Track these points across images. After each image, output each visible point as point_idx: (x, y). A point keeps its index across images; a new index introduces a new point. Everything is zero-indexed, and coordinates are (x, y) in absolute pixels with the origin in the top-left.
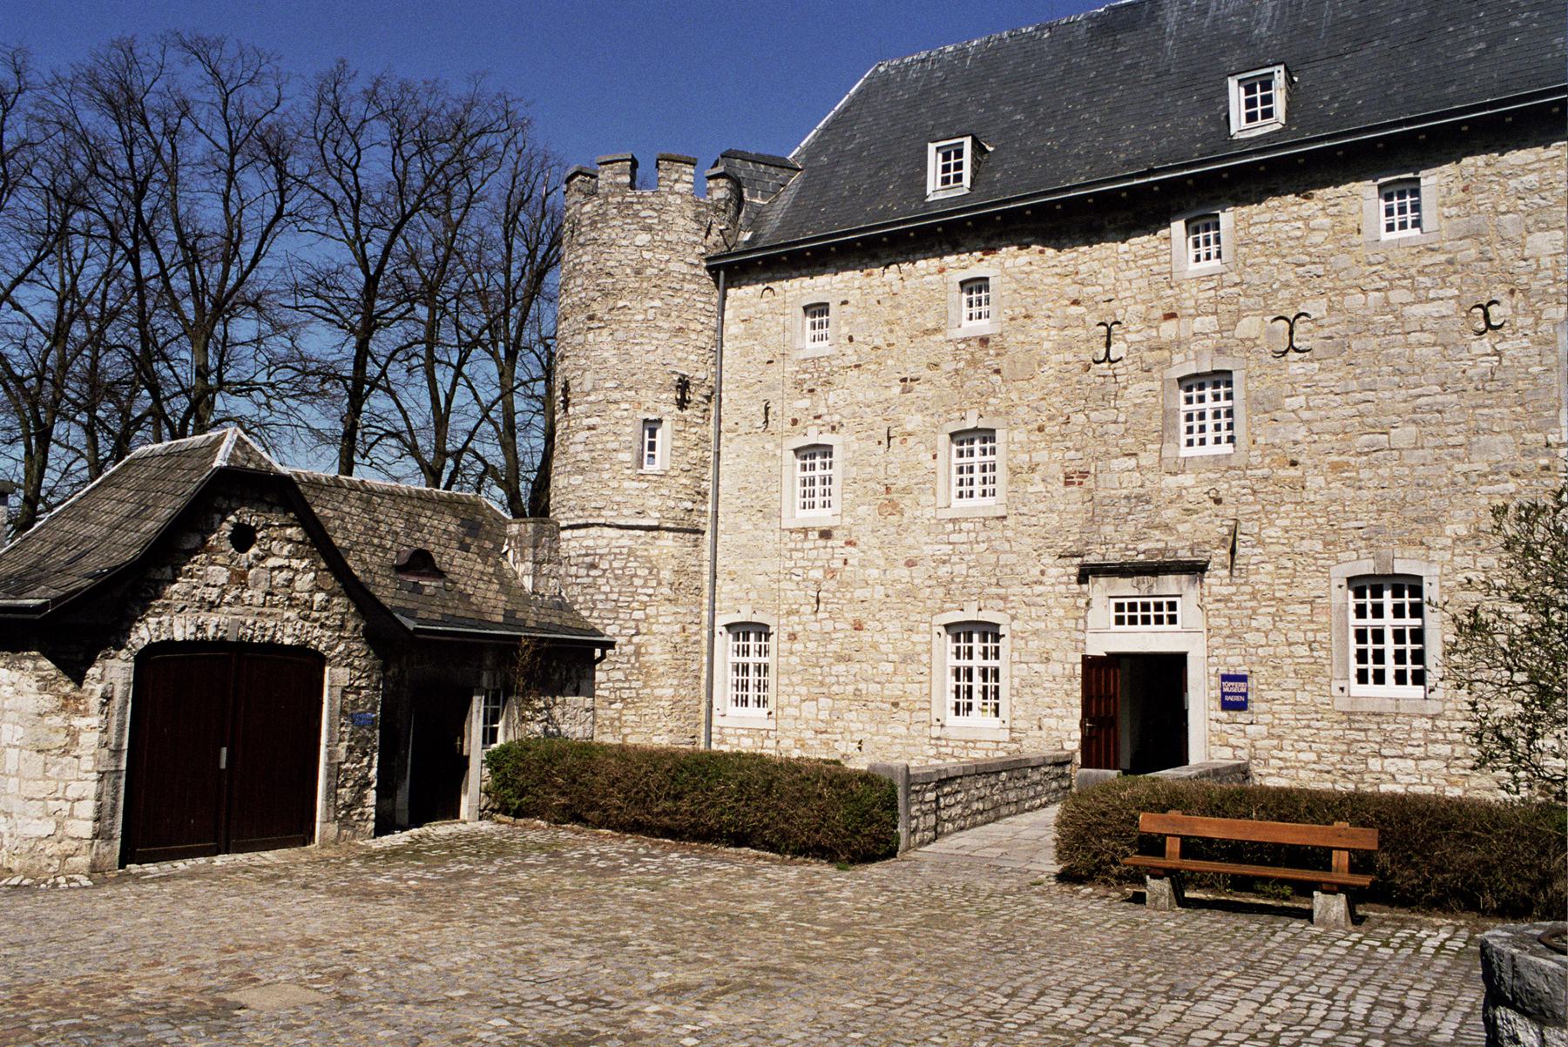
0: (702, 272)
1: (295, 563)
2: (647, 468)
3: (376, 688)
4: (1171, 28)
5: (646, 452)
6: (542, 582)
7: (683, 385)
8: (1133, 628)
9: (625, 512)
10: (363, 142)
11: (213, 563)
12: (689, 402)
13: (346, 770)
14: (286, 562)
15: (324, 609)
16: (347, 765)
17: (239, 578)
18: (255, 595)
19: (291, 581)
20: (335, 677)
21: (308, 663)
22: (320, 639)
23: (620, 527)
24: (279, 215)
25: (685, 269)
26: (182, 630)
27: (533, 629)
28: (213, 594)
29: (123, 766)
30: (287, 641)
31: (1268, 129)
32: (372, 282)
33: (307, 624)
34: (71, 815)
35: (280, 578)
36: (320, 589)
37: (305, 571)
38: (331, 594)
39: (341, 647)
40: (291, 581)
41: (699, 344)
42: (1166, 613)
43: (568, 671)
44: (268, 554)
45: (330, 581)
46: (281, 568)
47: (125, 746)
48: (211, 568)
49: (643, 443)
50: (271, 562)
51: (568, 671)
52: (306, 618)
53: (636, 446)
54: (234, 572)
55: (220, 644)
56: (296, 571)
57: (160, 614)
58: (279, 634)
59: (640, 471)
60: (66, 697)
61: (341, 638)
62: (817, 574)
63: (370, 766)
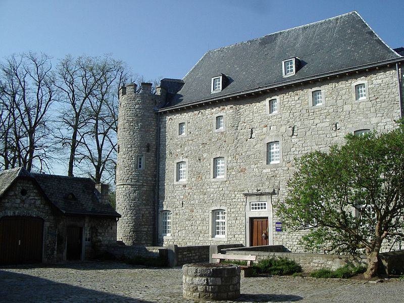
1: (36, 198)
4: (278, 43)
7: (148, 146)
8: (256, 210)
10: (74, 77)
11: (17, 198)
17: (23, 201)
18: (26, 206)
19: (35, 202)
20: (47, 224)
22: (42, 215)
24: (50, 100)
27: (99, 213)
28: (17, 205)
31: (291, 75)
32: (78, 115)
36: (42, 204)
37: (39, 200)
42: (262, 206)
44: (30, 196)
46: (33, 199)
52: (39, 211)
55: (19, 216)
56: (36, 200)
62: (182, 197)
63: (55, 245)
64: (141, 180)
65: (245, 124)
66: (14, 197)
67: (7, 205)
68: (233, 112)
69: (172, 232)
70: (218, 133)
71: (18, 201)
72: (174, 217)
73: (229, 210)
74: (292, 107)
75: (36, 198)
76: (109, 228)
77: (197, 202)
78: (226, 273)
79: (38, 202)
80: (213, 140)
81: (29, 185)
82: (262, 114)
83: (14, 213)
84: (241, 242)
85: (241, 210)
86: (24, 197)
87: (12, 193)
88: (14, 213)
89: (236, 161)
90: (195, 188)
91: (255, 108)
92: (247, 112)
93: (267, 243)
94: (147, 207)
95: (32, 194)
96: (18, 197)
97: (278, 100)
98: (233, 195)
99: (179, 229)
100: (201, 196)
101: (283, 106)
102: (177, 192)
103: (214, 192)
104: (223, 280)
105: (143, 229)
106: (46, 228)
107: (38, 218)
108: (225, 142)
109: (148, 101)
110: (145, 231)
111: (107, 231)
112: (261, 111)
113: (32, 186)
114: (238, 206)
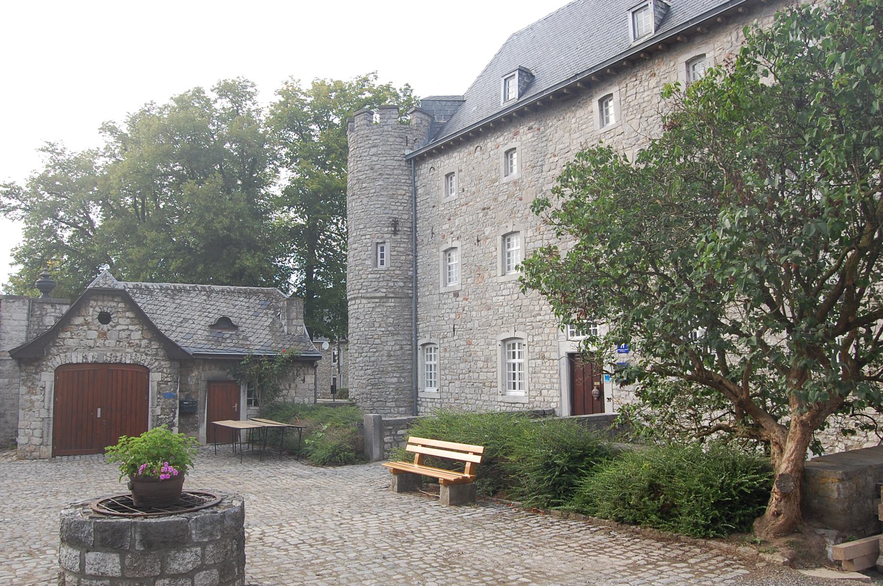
0: (403, 164)
1: (131, 327)
2: (380, 267)
3: (176, 382)
5: (379, 259)
6: (293, 329)
7: (395, 223)
9: (369, 290)
11: (89, 329)
12: (399, 231)
13: (161, 419)
14: (126, 327)
15: (147, 347)
16: (162, 416)
18: (111, 342)
19: (129, 335)
20: (155, 377)
21: (146, 371)
22: (145, 360)
23: (368, 298)
25: (395, 163)
26: (76, 358)
28: (91, 343)
29: (52, 416)
30: (128, 362)
33: (138, 354)
34: (33, 436)
35: (124, 335)
36: (144, 338)
37: (137, 330)
38: (150, 340)
39: (157, 364)
40: (129, 335)
41: (403, 201)
43: (298, 371)
44: (118, 324)
45: (149, 336)
47: (52, 407)
48: (89, 332)
49: (377, 254)
50: (119, 328)
51: (298, 371)
52: (138, 351)
53: (374, 256)
54: (100, 333)
56: (132, 331)
57: (66, 352)
58: (124, 359)
59: (375, 269)
60: (29, 387)
61: (156, 360)
62: (453, 316)
63: (174, 417)
64: (382, 287)
65: (556, 159)
66: (85, 327)
67: (70, 342)
68: (533, 136)
69: (438, 384)
70: (507, 184)
71: (93, 334)
72: (442, 355)
73: (530, 339)
74: (645, 105)
75: (131, 327)
76: (299, 380)
77: (477, 325)
78: (138, 537)
79: (136, 336)
80: (500, 199)
81: (115, 304)
82: (587, 130)
83: (85, 357)
84: (553, 405)
85: (551, 337)
86: (105, 327)
87: (79, 320)
88: (85, 357)
89: (539, 237)
90: (473, 297)
91: (574, 120)
92: (560, 133)
93: (603, 411)
94: (395, 337)
95: (121, 321)
96: (93, 327)
97: (616, 97)
98: (537, 308)
99: (449, 377)
100: (484, 313)
101: (624, 107)
102: (446, 307)
103: (505, 304)
104: (127, 562)
105: (389, 380)
106: (153, 387)
107: (136, 365)
108: (521, 199)
109: (391, 139)
110: (393, 384)
111: (293, 385)
112: (584, 127)
113: (121, 305)
114: (547, 330)
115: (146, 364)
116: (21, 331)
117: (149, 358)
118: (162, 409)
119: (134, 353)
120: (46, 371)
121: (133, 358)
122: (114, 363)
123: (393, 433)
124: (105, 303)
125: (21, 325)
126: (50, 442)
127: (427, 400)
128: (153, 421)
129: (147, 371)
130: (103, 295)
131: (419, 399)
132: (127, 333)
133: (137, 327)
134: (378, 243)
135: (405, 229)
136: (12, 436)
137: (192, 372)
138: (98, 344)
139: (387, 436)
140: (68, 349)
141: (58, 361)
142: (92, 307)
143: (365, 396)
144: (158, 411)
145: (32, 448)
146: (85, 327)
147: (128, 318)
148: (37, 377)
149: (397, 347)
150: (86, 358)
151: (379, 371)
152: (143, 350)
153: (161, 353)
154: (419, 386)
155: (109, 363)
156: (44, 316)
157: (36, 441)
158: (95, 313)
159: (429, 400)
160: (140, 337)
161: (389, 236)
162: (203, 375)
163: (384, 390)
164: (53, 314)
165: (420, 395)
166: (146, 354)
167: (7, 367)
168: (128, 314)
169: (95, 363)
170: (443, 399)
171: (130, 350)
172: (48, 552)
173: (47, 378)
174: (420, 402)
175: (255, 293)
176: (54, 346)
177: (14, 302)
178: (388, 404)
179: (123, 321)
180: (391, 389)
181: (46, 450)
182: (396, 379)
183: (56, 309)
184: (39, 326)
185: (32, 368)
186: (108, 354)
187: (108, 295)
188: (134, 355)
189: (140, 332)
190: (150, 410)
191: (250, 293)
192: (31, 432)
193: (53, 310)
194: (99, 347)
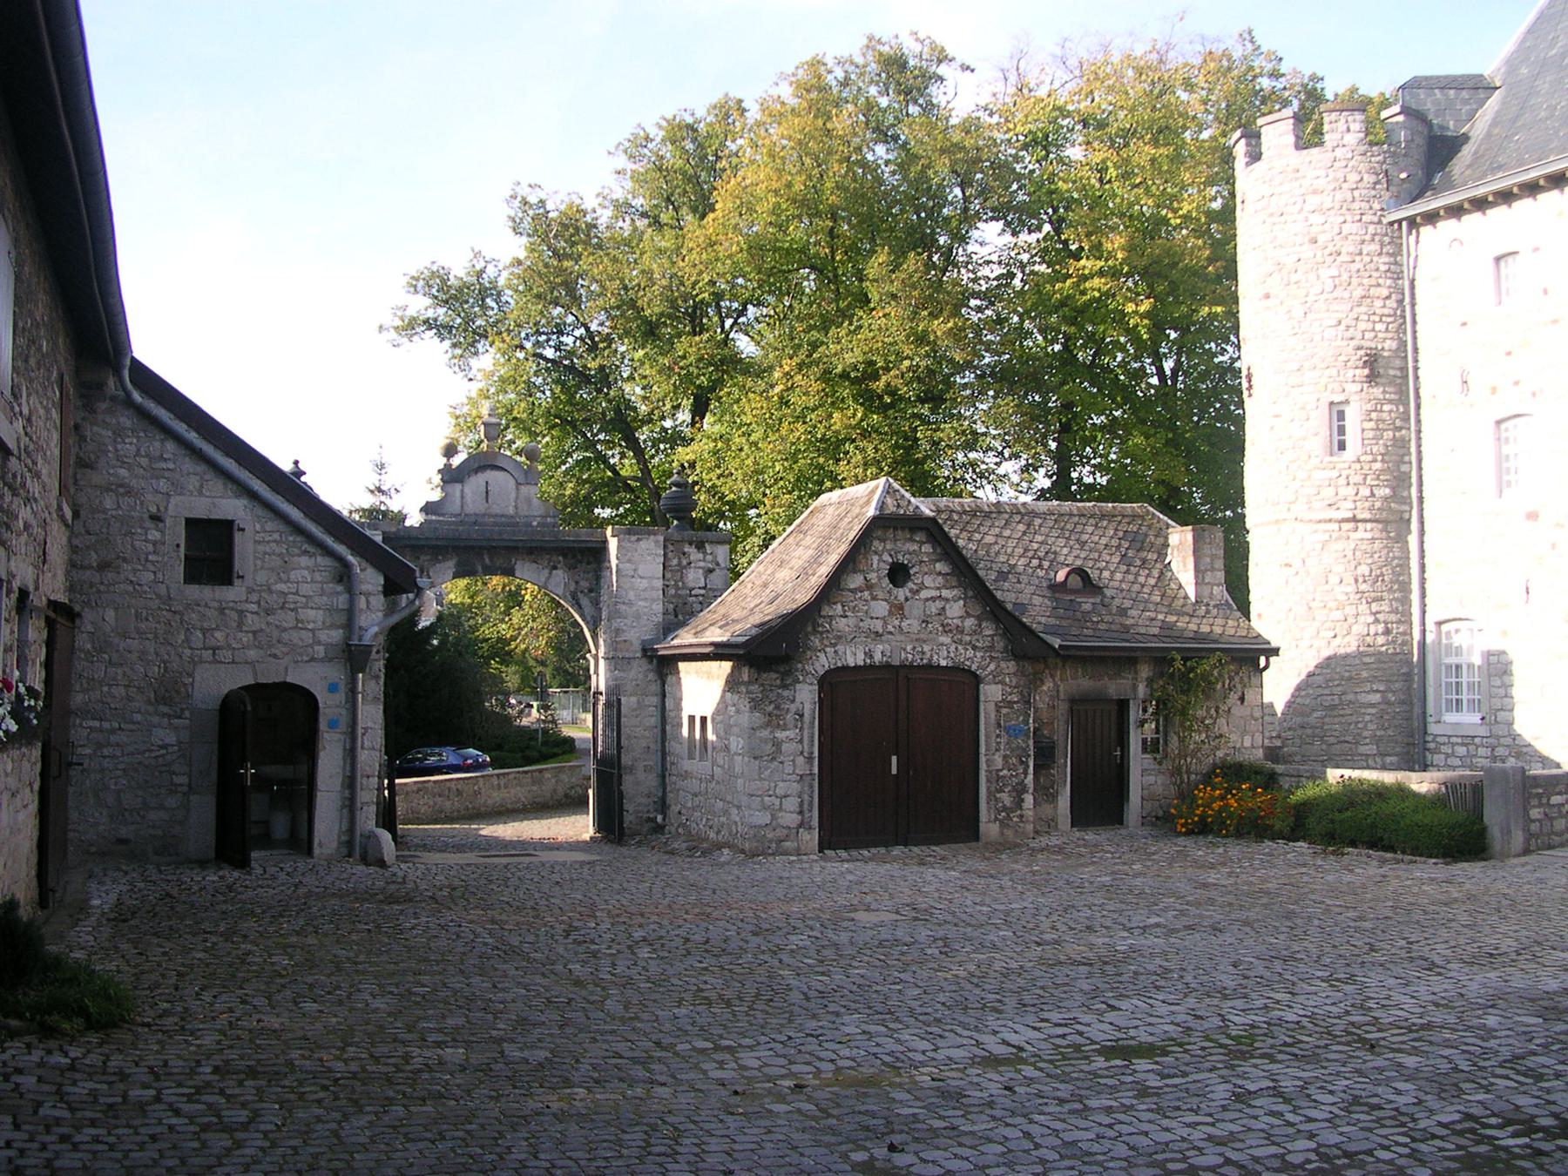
1: (945, 593)
11: (874, 598)
13: (1004, 777)
16: (1005, 772)
18: (912, 624)
20: (991, 693)
26: (854, 656)
29: (816, 770)
30: (943, 663)
34: (781, 809)
35: (933, 608)
36: (968, 615)
39: (992, 667)
40: (943, 609)
44: (922, 587)
45: (978, 610)
47: (816, 754)
48: (873, 603)
50: (924, 594)
52: (960, 642)
54: (892, 605)
56: (947, 600)
58: (935, 657)
61: (992, 658)
63: (1026, 773)
71: (881, 608)
79: (955, 610)
81: (916, 547)
83: (869, 654)
86: (901, 593)
87: (855, 581)
88: (869, 654)
95: (928, 581)
96: (881, 595)
107: (957, 670)
110: (1372, 705)
113: (927, 548)
115: (974, 668)
116: (653, 600)
117: (979, 654)
118: (1005, 757)
119: (954, 646)
120: (804, 681)
121: (952, 655)
122: (919, 666)
123: (1544, 801)
124: (899, 544)
125: (653, 588)
126: (815, 823)
127: (1454, 740)
128: (988, 781)
129: (976, 680)
130: (895, 529)
131: (1429, 738)
132: (939, 604)
133: (955, 592)
134: (1332, 403)
135: (1392, 372)
136: (648, 812)
137: (1042, 682)
138: (890, 628)
139: (1534, 807)
140: (840, 637)
141: (823, 662)
142: (876, 553)
143: (1309, 731)
144: (998, 761)
145: (781, 833)
146: (866, 593)
147: (940, 574)
148: (786, 693)
149: (1381, 628)
150: (871, 657)
151: (1342, 678)
152: (968, 638)
153: (1000, 645)
154: (1430, 709)
155: (911, 666)
156: (685, 567)
157: (791, 819)
158: (882, 565)
159: (1459, 740)
160: (961, 613)
161: (1357, 387)
162: (1061, 689)
163: (1354, 718)
164: (702, 564)
165: (1433, 729)
166: (974, 648)
167: (632, 674)
168: (939, 566)
169: (887, 667)
170: (1498, 738)
171: (945, 639)
172: (34, 1080)
173: (806, 695)
174: (1432, 746)
175: (1110, 516)
176: (815, 632)
177: (638, 540)
178: (1362, 749)
179: (931, 581)
180: (1367, 718)
181: (809, 837)
182: (1379, 695)
183: (705, 553)
184: (677, 588)
185: (774, 676)
186: (909, 648)
187: (903, 529)
188: (952, 649)
189: (962, 602)
190: (983, 759)
191: (1103, 516)
192: (777, 802)
193: (701, 556)
194: (891, 633)
